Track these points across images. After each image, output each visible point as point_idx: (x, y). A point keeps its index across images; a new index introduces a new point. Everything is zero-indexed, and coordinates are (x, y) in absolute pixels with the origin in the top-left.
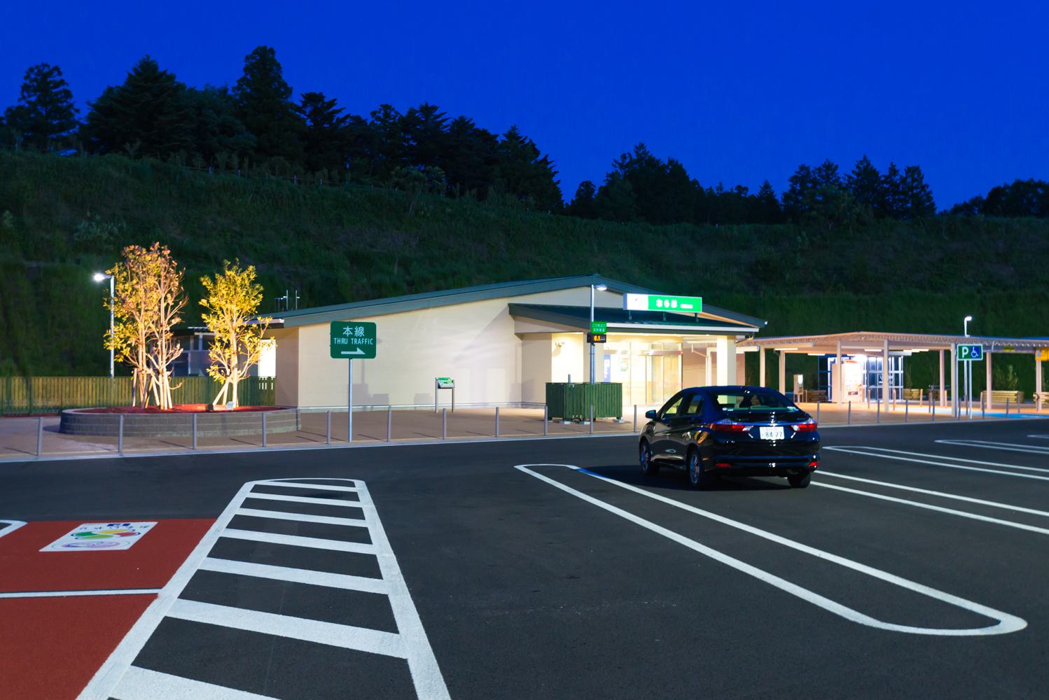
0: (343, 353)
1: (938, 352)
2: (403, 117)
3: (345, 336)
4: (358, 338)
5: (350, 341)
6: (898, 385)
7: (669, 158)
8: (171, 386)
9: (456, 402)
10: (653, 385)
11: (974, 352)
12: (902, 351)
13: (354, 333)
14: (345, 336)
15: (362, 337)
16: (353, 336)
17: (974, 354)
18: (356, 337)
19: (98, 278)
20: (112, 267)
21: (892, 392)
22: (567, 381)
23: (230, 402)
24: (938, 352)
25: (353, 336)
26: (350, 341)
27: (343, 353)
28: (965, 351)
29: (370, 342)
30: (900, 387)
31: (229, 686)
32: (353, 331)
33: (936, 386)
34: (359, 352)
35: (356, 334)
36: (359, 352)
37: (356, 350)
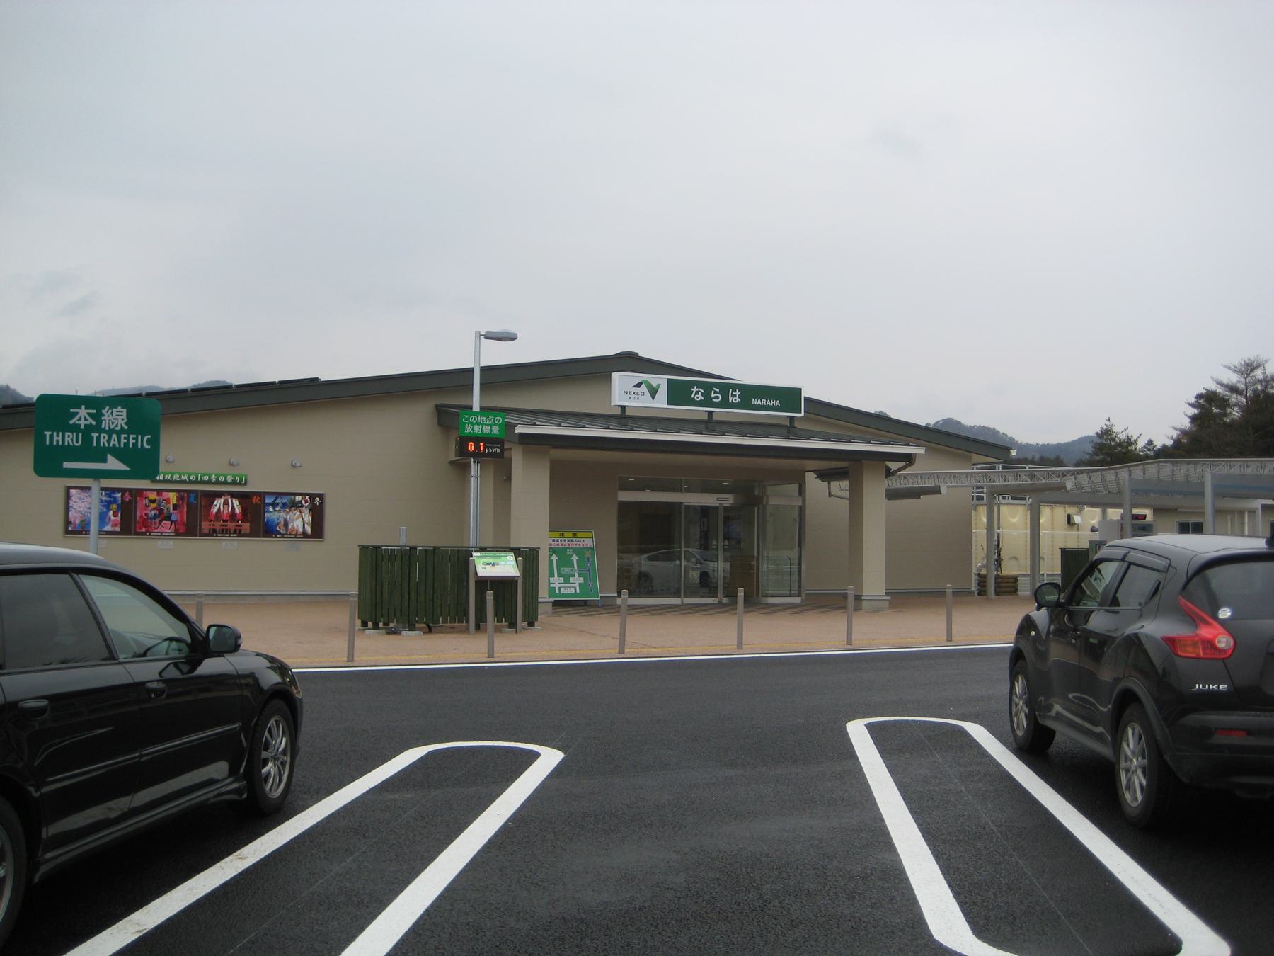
0: (66, 465)
4: (110, 432)
5: (87, 439)
6: (845, 596)
8: (714, 595)
13: (99, 422)
14: (75, 428)
15: (122, 431)
18: (104, 431)
20: (1246, 410)
21: (108, 533)
23: (1020, 663)
26: (87, 439)
27: (66, 465)
29: (143, 442)
30: (851, 593)
31: (428, 913)
32: (98, 417)
34: (113, 463)
36: (113, 463)
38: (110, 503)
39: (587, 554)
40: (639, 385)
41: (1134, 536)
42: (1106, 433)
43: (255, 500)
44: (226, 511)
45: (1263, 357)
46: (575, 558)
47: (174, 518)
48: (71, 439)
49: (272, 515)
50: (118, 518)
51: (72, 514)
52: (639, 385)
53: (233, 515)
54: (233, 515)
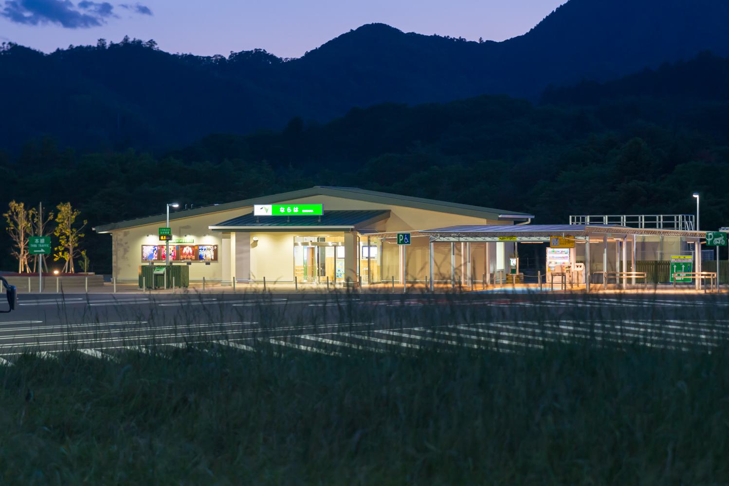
1: (645, 227)
2: (549, 247)
3: (36, 244)
4: (42, 244)
5: (38, 246)
7: (111, 42)
9: (296, 265)
10: (369, 262)
11: (406, 238)
12: (454, 254)
14: (36, 244)
16: (39, 243)
17: (406, 241)
19: (93, 229)
22: (344, 259)
24: (645, 227)
25: (39, 243)
26: (38, 246)
28: (401, 237)
32: (39, 241)
33: (508, 313)
35: (41, 242)
37: (41, 250)
38: (154, 250)
39: (689, 265)
40: (262, 208)
41: (695, 284)
42: (58, 50)
43: (196, 248)
44: (187, 252)
45: (156, 42)
46: (683, 266)
47: (172, 255)
48: (35, 246)
49: (201, 253)
50: (157, 255)
51: (144, 254)
52: (262, 208)
53: (189, 254)
54: (189, 254)
